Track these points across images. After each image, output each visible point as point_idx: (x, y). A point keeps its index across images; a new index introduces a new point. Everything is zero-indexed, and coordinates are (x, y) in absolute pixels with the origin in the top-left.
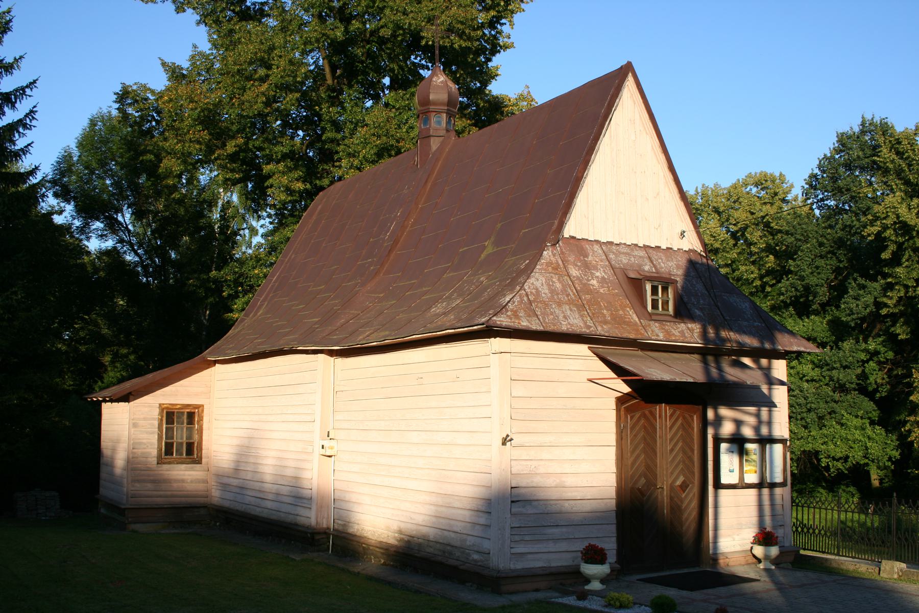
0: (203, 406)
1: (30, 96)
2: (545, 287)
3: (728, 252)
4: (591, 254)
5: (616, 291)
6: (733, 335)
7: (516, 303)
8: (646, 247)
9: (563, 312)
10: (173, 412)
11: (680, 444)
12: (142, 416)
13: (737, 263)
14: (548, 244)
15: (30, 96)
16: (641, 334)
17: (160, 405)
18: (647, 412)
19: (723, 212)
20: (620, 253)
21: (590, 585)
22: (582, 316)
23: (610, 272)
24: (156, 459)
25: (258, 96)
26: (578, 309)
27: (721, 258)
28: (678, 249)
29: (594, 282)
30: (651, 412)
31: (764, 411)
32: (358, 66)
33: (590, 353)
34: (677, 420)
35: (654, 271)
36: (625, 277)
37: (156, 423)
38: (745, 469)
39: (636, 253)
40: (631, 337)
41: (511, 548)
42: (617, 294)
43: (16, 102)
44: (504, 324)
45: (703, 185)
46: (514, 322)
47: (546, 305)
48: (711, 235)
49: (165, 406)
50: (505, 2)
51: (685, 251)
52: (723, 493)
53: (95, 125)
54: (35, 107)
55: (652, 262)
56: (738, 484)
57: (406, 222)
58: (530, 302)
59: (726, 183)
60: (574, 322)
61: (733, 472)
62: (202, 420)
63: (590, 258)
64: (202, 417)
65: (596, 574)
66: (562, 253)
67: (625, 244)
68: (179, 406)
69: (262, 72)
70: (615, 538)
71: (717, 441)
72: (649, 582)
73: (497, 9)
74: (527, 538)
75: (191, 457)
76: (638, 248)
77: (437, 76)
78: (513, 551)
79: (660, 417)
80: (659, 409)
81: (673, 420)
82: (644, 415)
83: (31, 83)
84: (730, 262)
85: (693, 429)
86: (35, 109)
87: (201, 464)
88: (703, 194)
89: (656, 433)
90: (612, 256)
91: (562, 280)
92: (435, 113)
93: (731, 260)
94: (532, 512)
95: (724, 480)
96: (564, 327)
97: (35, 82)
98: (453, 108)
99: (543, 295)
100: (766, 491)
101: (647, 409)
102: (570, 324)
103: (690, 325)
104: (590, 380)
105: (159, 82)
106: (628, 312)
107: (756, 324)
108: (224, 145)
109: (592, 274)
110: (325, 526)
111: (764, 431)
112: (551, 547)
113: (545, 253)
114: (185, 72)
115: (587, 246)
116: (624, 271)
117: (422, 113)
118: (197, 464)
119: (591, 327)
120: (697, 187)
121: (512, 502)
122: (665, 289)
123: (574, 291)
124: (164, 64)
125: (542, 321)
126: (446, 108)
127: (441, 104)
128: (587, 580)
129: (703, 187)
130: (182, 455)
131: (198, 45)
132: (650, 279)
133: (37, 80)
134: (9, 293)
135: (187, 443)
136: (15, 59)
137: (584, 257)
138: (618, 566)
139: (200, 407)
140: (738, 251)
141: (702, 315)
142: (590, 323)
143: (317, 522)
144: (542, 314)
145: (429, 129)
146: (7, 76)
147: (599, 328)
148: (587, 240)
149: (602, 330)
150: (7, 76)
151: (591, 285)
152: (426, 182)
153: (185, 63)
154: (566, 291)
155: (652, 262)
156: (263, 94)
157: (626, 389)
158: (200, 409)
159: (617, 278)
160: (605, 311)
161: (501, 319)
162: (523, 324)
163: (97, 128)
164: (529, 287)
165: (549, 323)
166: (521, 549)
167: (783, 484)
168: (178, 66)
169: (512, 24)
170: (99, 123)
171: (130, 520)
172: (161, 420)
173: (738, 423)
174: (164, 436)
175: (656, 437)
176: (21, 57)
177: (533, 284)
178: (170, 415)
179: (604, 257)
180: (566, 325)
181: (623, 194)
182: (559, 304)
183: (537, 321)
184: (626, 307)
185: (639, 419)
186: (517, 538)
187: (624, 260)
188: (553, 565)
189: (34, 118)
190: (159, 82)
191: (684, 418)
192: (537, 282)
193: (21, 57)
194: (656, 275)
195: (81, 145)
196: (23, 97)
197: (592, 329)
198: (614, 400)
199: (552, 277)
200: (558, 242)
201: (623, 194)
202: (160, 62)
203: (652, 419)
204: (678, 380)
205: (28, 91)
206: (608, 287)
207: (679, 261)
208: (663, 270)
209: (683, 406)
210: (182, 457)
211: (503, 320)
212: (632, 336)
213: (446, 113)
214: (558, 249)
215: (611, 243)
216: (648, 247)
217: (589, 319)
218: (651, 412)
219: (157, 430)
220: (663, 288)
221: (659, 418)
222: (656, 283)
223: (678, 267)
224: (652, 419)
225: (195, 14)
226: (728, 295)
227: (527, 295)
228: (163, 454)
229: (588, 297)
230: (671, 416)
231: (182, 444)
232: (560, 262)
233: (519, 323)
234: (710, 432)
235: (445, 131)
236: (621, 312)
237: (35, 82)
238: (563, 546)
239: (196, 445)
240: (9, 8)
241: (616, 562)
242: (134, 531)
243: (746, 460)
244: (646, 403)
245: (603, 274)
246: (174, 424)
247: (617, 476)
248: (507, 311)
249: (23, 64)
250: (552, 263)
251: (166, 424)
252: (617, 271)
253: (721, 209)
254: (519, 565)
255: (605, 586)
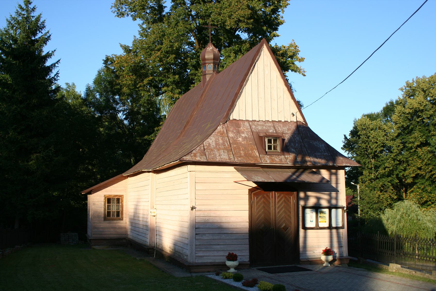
0: (123, 195)
1: (58, 67)
2: (214, 142)
3: (428, 111)
4: (242, 126)
5: (251, 142)
6: (312, 159)
7: (197, 150)
8: (273, 121)
9: (219, 153)
10: (111, 198)
11: (283, 210)
12: (97, 201)
13: (434, 116)
14: (221, 123)
15: (58, 67)
16: (258, 161)
17: (104, 195)
18: (265, 195)
19: (426, 90)
20: (258, 125)
21: (230, 270)
22: (228, 154)
23: (250, 134)
24: (103, 218)
25: (156, 58)
26: (228, 152)
27: (425, 114)
28: (291, 121)
29: (240, 139)
30: (267, 196)
31: (334, 194)
32: (207, 39)
33: (235, 170)
34: (281, 198)
35: (275, 132)
36: (258, 136)
37: (103, 203)
38: (319, 220)
39: (267, 124)
40: (252, 163)
41: (196, 254)
42: (251, 144)
43: (52, 70)
44: (187, 159)
45: (417, 77)
46: (193, 159)
47: (212, 150)
48: (418, 103)
49: (107, 196)
50: (277, 1)
51: (295, 122)
52: (309, 232)
53: (100, 73)
54: (58, 71)
55: (275, 128)
56: (315, 227)
57: (192, 114)
58: (204, 149)
59: (428, 75)
60: (224, 157)
61: (313, 222)
62: (123, 202)
63: (241, 128)
64: (123, 200)
65: (230, 265)
66: (227, 126)
67: (262, 121)
68: (113, 196)
69: (158, 47)
70: (248, 251)
71: (304, 208)
72: (262, 270)
73: (274, 5)
74: (203, 249)
75: (118, 217)
76: (269, 122)
77: (209, 47)
78: (197, 255)
79: (272, 197)
80: (272, 194)
81: (279, 198)
82: (264, 197)
83: (58, 61)
84: (429, 116)
85: (290, 202)
86: (58, 72)
87: (123, 220)
88: (417, 82)
89: (270, 204)
90: (253, 127)
91: (223, 139)
92: (208, 64)
93: (430, 115)
94: (206, 239)
95: (308, 225)
96: (218, 160)
97: (59, 61)
98: (217, 61)
99: (212, 146)
100: (334, 231)
101: (265, 194)
102: (221, 158)
103: (286, 156)
104: (235, 182)
105: (121, 52)
106: (254, 151)
107: (325, 154)
108: (143, 80)
109: (240, 135)
110: (153, 246)
111: (334, 202)
112: (216, 254)
113: (219, 127)
114: (130, 48)
115: (241, 123)
116: (258, 133)
117: (203, 64)
118: (121, 220)
119: (232, 159)
120: (413, 78)
121: (196, 234)
122: (275, 141)
123: (229, 143)
124: (121, 46)
125: (207, 157)
126: (213, 61)
127: (211, 59)
128: (229, 268)
129: (417, 78)
130: (115, 217)
131: (136, 36)
132: (267, 136)
133: (60, 60)
134: (48, 150)
135: (117, 212)
136: (52, 51)
137: (238, 128)
138: (249, 263)
139: (122, 196)
140: (434, 110)
141: (295, 151)
142: (232, 157)
143: (150, 244)
144: (208, 154)
145: (205, 71)
146: (49, 59)
147: (236, 159)
148: (242, 120)
149: (237, 160)
150: (49, 59)
151: (238, 140)
152: (202, 95)
153: (130, 44)
154: (224, 144)
155: (275, 128)
156: (158, 56)
157: (255, 185)
158: (122, 197)
159: (253, 137)
160: (242, 152)
161: (187, 157)
162: (197, 159)
163: (101, 74)
164: (206, 143)
165: (211, 158)
166: (201, 254)
167: (343, 227)
168: (127, 46)
169: (283, 12)
170: (102, 72)
171: (93, 244)
172: (105, 202)
173: (318, 199)
174: (107, 209)
175: (270, 206)
176: (55, 51)
177: (208, 141)
178: (109, 200)
179: (249, 127)
180: (219, 159)
181: (261, 98)
182: (219, 150)
183: (205, 157)
184: (254, 149)
185: (261, 199)
186: (198, 249)
187: (260, 128)
188: (217, 261)
189: (58, 76)
190: (121, 52)
191: (286, 197)
192: (211, 141)
193: (55, 51)
194: (275, 134)
195: (95, 83)
196: (55, 68)
197: (232, 160)
198: (248, 190)
199: (219, 138)
200: (226, 122)
201: (261, 98)
202: (120, 45)
203: (268, 198)
204: (266, 181)
205: (56, 65)
206: (247, 141)
207: (290, 127)
208: (279, 131)
209: (284, 192)
210: (110, 217)
211: (188, 158)
212: (252, 162)
213: (213, 63)
214: (226, 125)
215: (255, 121)
216: (275, 121)
217: (232, 155)
218: (267, 196)
219: (103, 206)
220: (274, 140)
221: (272, 198)
222: (270, 138)
223: (288, 130)
224: (268, 198)
225: (141, 20)
226: (313, 141)
227: (204, 146)
228: (106, 216)
229: (235, 146)
230: (278, 197)
231: (114, 212)
232: (225, 131)
233: (195, 159)
234: (302, 203)
235: (212, 72)
236: (250, 152)
237: (59, 61)
238: (222, 253)
239: (120, 212)
240: (48, 31)
241: (249, 261)
242: (94, 249)
243: (320, 217)
244: (265, 191)
245: (246, 135)
246: (110, 203)
247: (249, 223)
248: (192, 154)
249: (55, 53)
250: (220, 132)
251: (107, 203)
252: (255, 134)
253: (425, 90)
254: (200, 261)
255: (236, 271)
